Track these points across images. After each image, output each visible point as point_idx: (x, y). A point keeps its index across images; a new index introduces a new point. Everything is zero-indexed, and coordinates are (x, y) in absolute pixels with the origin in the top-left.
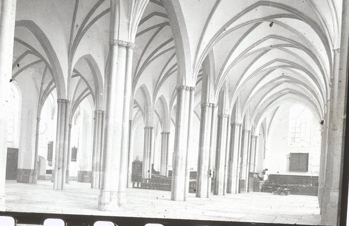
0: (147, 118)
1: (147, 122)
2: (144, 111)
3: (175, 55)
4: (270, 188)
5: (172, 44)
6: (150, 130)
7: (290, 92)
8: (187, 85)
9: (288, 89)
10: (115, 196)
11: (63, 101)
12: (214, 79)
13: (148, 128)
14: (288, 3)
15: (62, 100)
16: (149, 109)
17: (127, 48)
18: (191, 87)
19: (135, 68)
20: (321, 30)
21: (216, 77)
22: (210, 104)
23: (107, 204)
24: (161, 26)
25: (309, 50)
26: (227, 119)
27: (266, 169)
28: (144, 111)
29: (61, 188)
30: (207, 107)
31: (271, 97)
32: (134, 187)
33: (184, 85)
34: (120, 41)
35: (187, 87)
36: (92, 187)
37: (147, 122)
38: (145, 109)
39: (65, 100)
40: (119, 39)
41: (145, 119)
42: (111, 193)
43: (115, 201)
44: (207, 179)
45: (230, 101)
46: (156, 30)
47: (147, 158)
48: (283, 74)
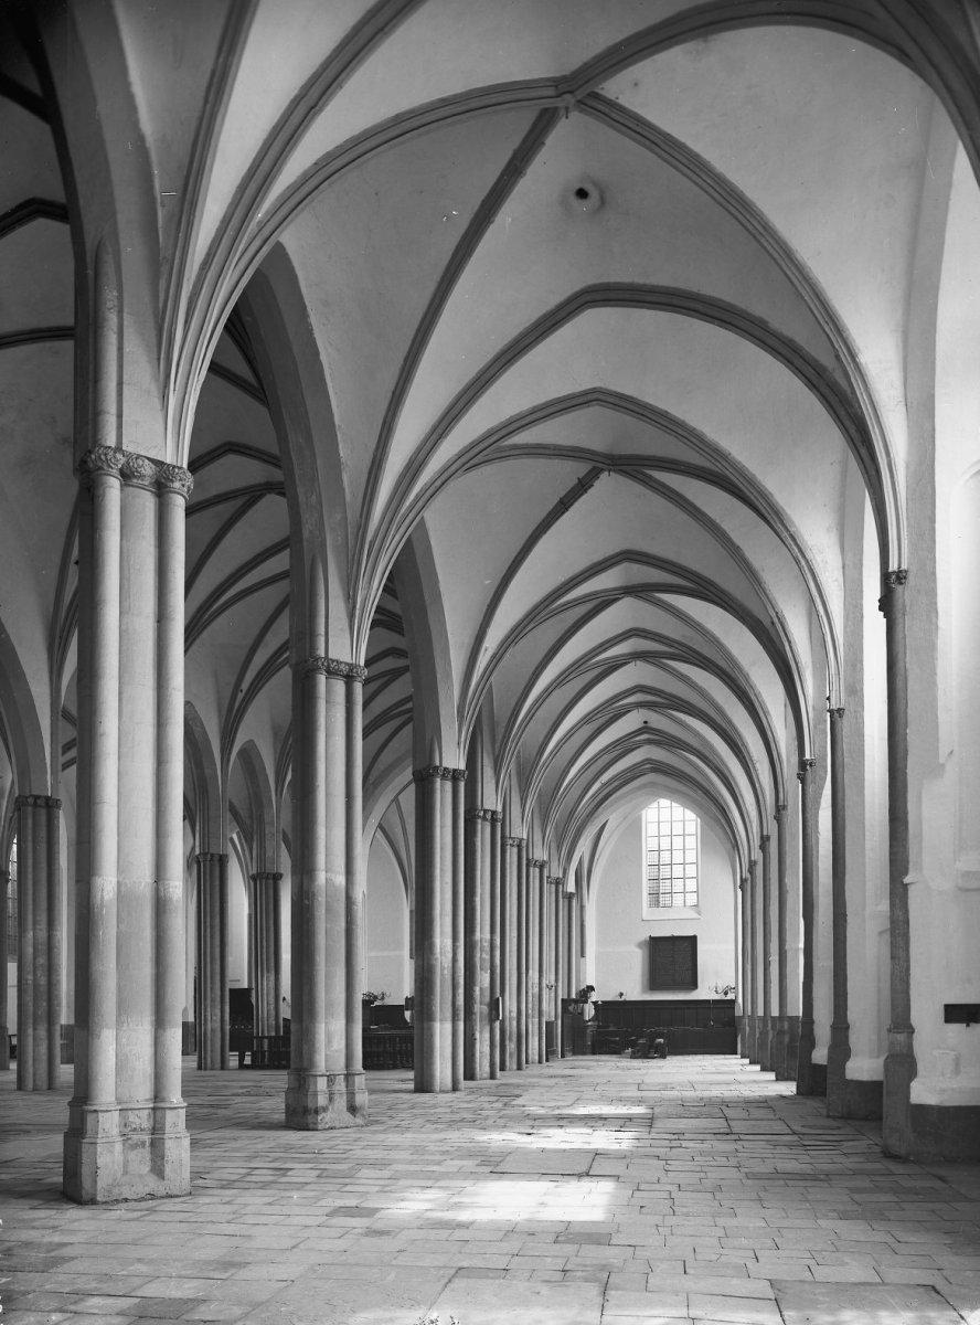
0: (262, 847)
1: (262, 859)
2: (248, 822)
3: (284, 607)
4: (615, 1042)
5: (279, 563)
6: (271, 881)
7: (654, 770)
8: (445, 765)
9: (648, 761)
10: (340, 1085)
11: (39, 801)
12: (493, 742)
13: (267, 878)
14: (580, 385)
15: (37, 797)
16: (267, 818)
17: (349, 679)
18: (455, 770)
19: (52, 596)
20: (771, 640)
21: (499, 737)
22: (485, 811)
23: (325, 1109)
24: (251, 496)
25: (729, 677)
26: (515, 850)
27: (588, 987)
28: (248, 822)
29: (45, 1086)
30: (479, 821)
31: (605, 785)
32: (242, 1066)
33: (438, 764)
34: (333, 661)
35: (445, 769)
36: (200, 1068)
37: (262, 859)
38: (251, 817)
39: (48, 799)
40: (330, 656)
41: (198, 828)
42: (331, 1079)
43: (341, 1103)
44: (488, 1028)
45: (522, 799)
46: (239, 502)
47: (268, 972)
48: (645, 722)
